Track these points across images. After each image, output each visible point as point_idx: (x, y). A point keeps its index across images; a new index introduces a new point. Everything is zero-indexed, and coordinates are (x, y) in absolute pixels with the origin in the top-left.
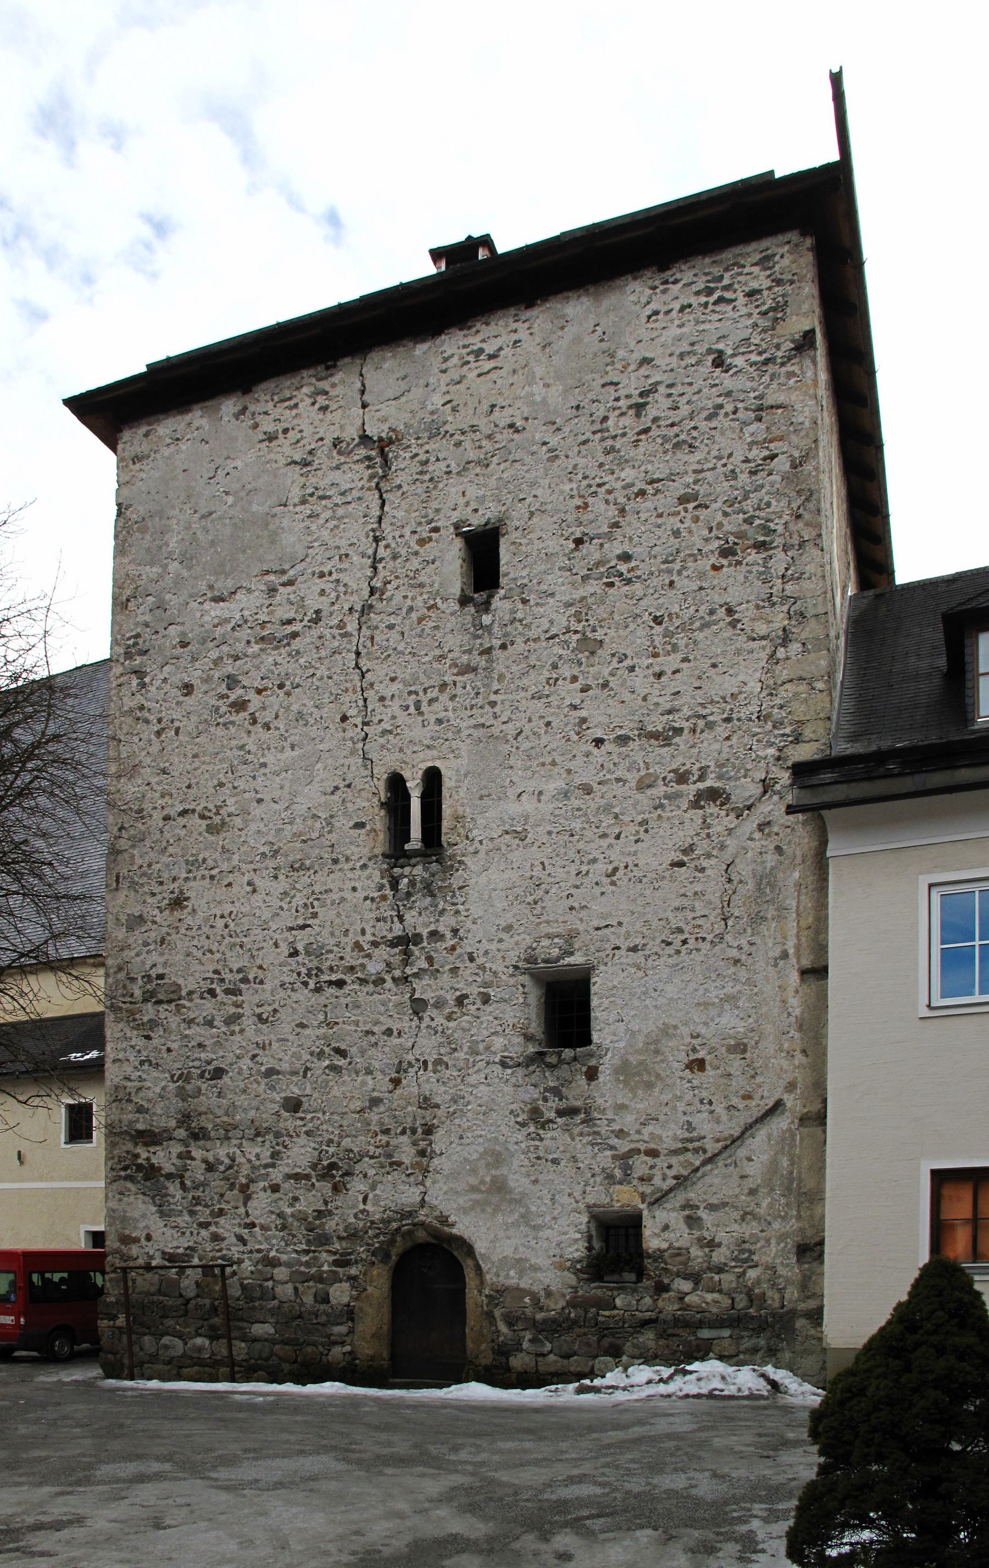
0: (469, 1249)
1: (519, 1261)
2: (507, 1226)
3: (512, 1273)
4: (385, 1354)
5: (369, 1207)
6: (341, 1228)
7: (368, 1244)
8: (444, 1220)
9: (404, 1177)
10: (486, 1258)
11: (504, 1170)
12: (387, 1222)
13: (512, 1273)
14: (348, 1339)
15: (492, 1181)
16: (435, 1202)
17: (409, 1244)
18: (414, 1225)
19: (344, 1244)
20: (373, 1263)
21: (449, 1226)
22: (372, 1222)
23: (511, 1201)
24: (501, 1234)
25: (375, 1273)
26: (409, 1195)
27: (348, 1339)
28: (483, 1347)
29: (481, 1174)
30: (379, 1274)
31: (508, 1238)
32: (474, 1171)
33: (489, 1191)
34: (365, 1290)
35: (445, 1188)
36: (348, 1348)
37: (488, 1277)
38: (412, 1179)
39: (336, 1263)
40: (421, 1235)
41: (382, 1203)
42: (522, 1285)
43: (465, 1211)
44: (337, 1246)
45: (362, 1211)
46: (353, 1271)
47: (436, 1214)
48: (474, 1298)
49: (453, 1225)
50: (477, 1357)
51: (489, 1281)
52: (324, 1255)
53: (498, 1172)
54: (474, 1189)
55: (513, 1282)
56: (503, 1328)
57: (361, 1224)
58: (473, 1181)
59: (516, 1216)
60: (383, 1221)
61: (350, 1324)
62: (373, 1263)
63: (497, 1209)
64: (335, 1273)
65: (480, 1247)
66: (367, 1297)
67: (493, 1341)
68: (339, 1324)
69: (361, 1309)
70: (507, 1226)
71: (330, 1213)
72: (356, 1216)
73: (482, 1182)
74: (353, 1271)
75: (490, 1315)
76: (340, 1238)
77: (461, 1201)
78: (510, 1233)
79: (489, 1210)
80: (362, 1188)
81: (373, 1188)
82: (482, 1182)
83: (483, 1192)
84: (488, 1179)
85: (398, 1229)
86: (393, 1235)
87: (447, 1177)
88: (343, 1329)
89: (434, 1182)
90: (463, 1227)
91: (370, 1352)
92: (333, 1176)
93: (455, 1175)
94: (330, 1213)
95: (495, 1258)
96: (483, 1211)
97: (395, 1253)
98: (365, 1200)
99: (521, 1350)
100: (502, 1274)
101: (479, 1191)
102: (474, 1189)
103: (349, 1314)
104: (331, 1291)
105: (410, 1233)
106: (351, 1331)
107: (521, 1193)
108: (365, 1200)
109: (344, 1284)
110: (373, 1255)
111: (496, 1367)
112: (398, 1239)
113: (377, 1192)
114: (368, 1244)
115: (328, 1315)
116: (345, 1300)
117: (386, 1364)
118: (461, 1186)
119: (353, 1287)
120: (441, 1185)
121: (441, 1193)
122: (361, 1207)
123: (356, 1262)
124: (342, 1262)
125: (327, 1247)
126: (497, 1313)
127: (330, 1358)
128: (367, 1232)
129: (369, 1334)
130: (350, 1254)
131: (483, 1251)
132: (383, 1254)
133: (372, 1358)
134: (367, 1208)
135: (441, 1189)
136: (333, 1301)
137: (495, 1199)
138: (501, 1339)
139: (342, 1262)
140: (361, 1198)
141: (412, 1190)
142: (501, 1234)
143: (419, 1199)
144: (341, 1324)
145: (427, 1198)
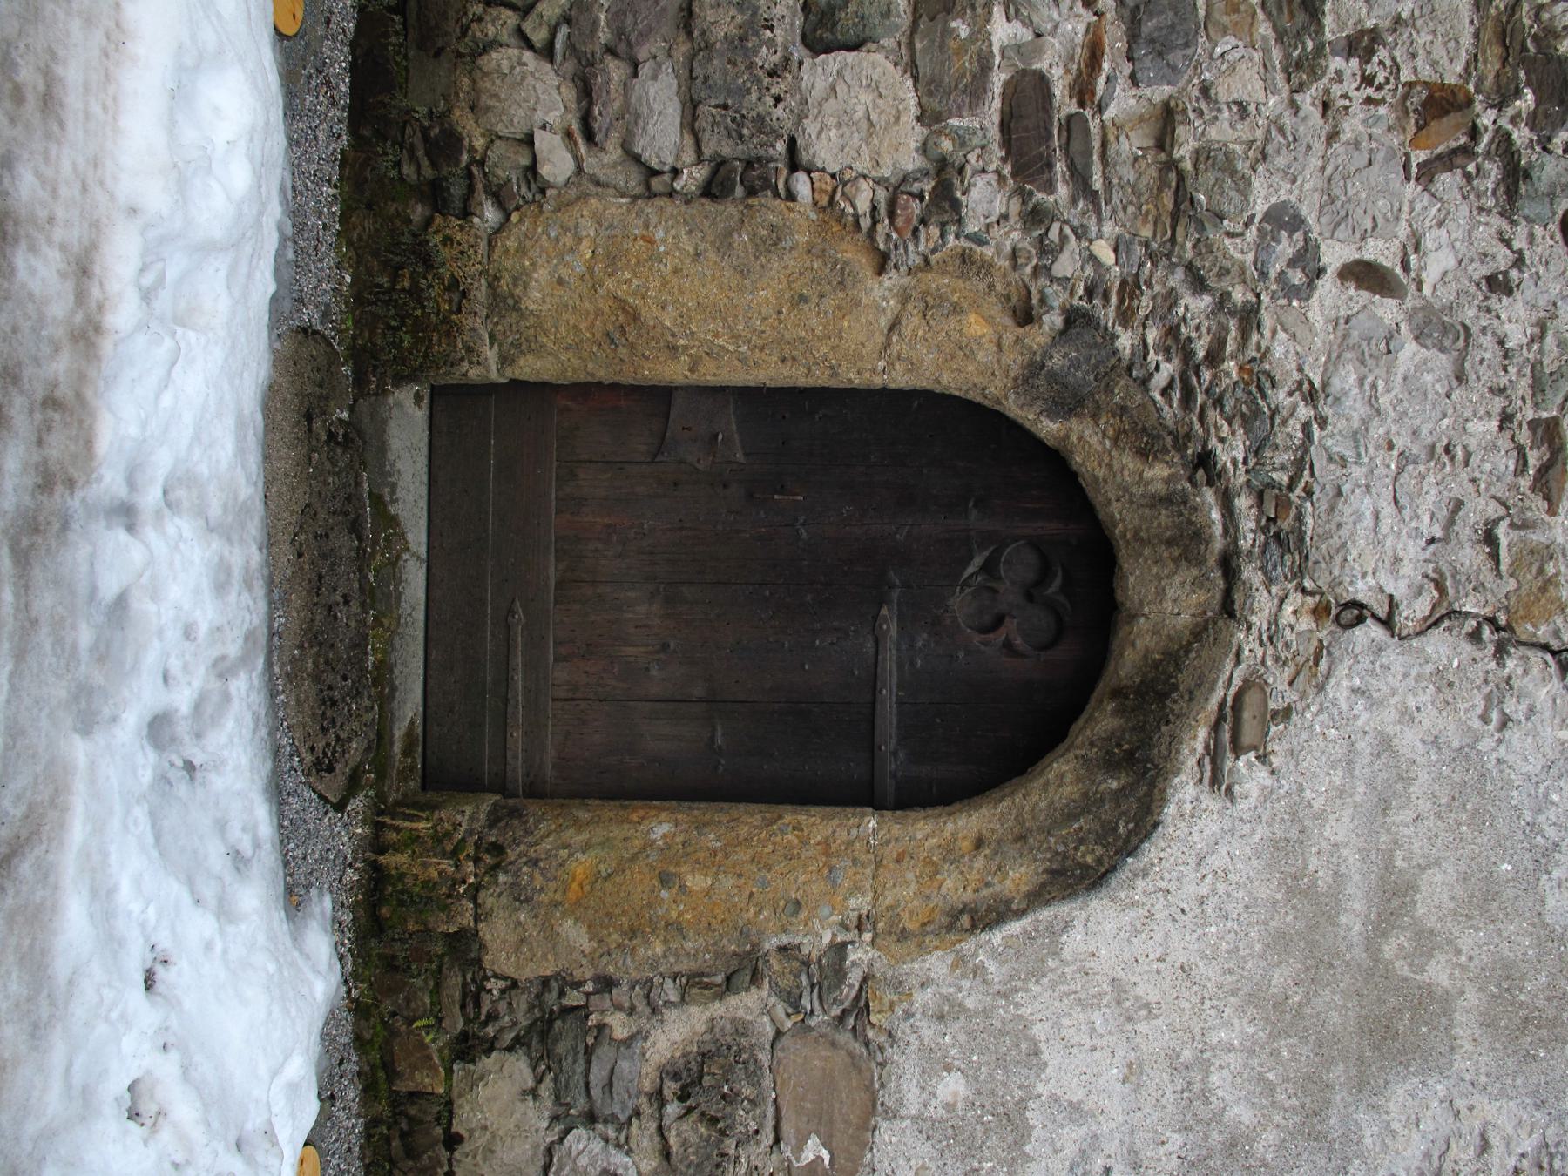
0: (1088, 863)
1: (1013, 1123)
2: (1190, 1071)
3: (952, 1087)
4: (529, 368)
6: (1223, 131)
7: (1131, 288)
8: (1237, 731)
9: (1480, 509)
10: (1035, 962)
11: (1472, 1053)
13: (952, 1087)
14: (606, 161)
15: (1429, 990)
16: (1339, 689)
17: (1120, 515)
18: (1229, 566)
19: (1130, 144)
20: (1025, 316)
21: (1214, 754)
22: (1249, 318)
23: (1315, 1087)
24: (1153, 1036)
25: (975, 326)
26: (1380, 539)
27: (606, 161)
28: (575, 934)
29: (1466, 941)
30: (964, 349)
31: (1133, 1073)
32: (1483, 899)
33: (1377, 970)
34: (882, 263)
35: (1409, 741)
36: (557, 164)
37: (937, 964)
38: (1470, 556)
39: (1028, 93)
40: (1163, 601)
41: (1346, 379)
42: (886, 1134)
43: (1283, 850)
44: (1123, 103)
45: (1307, 259)
46: (985, 198)
47: (1278, 680)
48: (837, 874)
49: (1217, 780)
50: (521, 897)
51: (914, 968)
52: (1075, 26)
53: (1465, 1027)
54: (1394, 895)
55: (907, 1086)
56: (676, 1032)
57: (1239, 251)
58: (1436, 893)
59: (1242, 1114)
60: (1258, 378)
61: (693, 177)
62: (1025, 316)
63: (1281, 1015)
64: (976, 92)
65: (1096, 930)
66: (844, 278)
67: (606, 984)
68: (691, 107)
69: (774, 241)
70: (1190, 1071)
71: (1302, 69)
72: (1283, 219)
73: (1426, 943)
74: (985, 198)
75: (744, 969)
76: (1167, 119)
77: (1340, 828)
78: (1159, 1076)
79: (1279, 978)
80: (1437, 263)
81: (1435, 327)
82: (1426, 943)
83: (1372, 946)
84: (1438, 973)
86: (1181, 440)
87: (1466, 753)
88: (663, 137)
89: (1442, 680)
90: (1205, 836)
91: (534, 299)
92: (1503, 97)
93: (1472, 790)
94: (1302, 69)
95: (1037, 1004)
96: (1280, 943)
97: (1087, 442)
98: (1366, 275)
99: (563, 1121)
100: (951, 1038)
101: (1382, 926)
102: (1394, 895)
103: (742, 177)
104: (876, 64)
105: (1186, 542)
106: (652, 181)
107: (1351, 1137)
108: (1366, 275)
109: (913, 134)
110: (1074, 318)
111: (472, 996)
112: (1159, 471)
113: (1409, 351)
114: (1131, 288)
115: (740, 44)
116: (824, 149)
117: (488, 367)
118: (1415, 831)
119: (897, 189)
120: (1429, 719)
121: (1387, 718)
122: (1334, 255)
123: (1036, 217)
124: (1035, 134)
125: (1115, 39)
126: (749, 1004)
127: (499, 59)
128: (1199, 284)
129: (616, 275)
130: (1079, 178)
131: (1074, 941)
132: (1085, 372)
133: (503, 303)
134: (1327, 286)
135: (1407, 717)
136: (818, 73)
137: (1335, 1008)
138: (619, 1026)
139: (1035, 134)
140: (1381, 251)
141: (1412, 550)
142: (1153, 1036)
143: (1361, 590)
144: (690, 124)
145: (1371, 631)
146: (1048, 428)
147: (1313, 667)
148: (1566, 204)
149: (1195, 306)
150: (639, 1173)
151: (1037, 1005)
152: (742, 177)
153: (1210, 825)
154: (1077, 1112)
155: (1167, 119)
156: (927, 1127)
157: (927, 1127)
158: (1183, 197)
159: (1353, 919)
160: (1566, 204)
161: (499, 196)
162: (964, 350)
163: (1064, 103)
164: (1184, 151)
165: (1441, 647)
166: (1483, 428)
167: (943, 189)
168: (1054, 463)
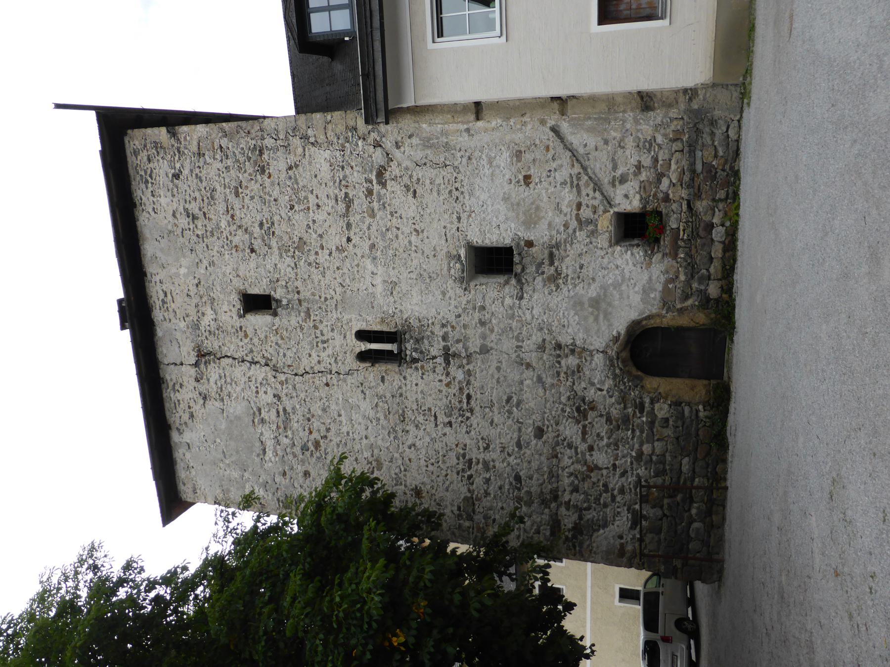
3: (652, 296)
5: (606, 387)
6: (618, 407)
8: (616, 339)
9: (587, 364)
11: (585, 300)
12: (615, 376)
16: (604, 344)
18: (618, 358)
22: (615, 386)
26: (599, 360)
31: (628, 297)
32: (586, 318)
33: (598, 309)
35: (595, 337)
36: (701, 407)
37: (654, 311)
38: (588, 358)
43: (611, 325)
44: (630, 410)
45: (608, 392)
46: (647, 400)
48: (669, 320)
49: (619, 333)
54: (596, 319)
55: (658, 295)
56: (689, 302)
58: (591, 319)
59: (615, 292)
60: (614, 379)
61: (683, 404)
62: (642, 387)
65: (634, 315)
71: (608, 413)
72: (611, 397)
73: (592, 313)
74: (647, 400)
80: (592, 391)
81: (593, 384)
82: (592, 313)
84: (590, 310)
85: (621, 370)
88: (687, 410)
90: (620, 325)
92: (585, 409)
94: (608, 413)
96: (610, 313)
97: (635, 371)
98: (601, 390)
102: (596, 319)
103: (677, 404)
105: (623, 362)
108: (601, 390)
113: (596, 381)
119: (658, 401)
122: (605, 392)
123: (641, 398)
126: (679, 306)
131: (637, 314)
136: (667, 415)
137: (603, 305)
139: (641, 407)
140: (600, 393)
146: (639, 373)
147: (607, 346)
148: (599, 607)
149: (622, 387)
150: (348, 658)
151: (642, 306)
152: (677, 404)
153: (620, 327)
154: (636, 292)
155: (625, 408)
156: (656, 290)
157: (656, 290)
158: (623, 399)
159: (601, 317)
160: (599, 607)
161: (709, 405)
162: (652, 382)
163: (637, 411)
164: (622, 405)
165: (592, 348)
166: (587, 373)
167: (652, 402)
168: (639, 368)
